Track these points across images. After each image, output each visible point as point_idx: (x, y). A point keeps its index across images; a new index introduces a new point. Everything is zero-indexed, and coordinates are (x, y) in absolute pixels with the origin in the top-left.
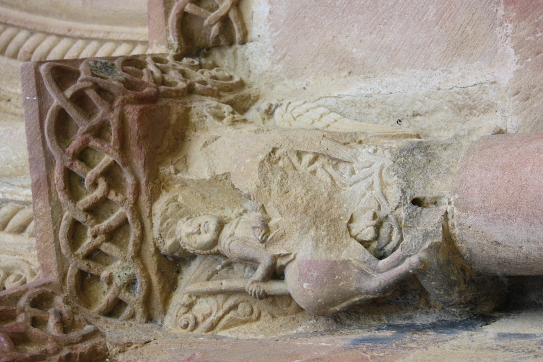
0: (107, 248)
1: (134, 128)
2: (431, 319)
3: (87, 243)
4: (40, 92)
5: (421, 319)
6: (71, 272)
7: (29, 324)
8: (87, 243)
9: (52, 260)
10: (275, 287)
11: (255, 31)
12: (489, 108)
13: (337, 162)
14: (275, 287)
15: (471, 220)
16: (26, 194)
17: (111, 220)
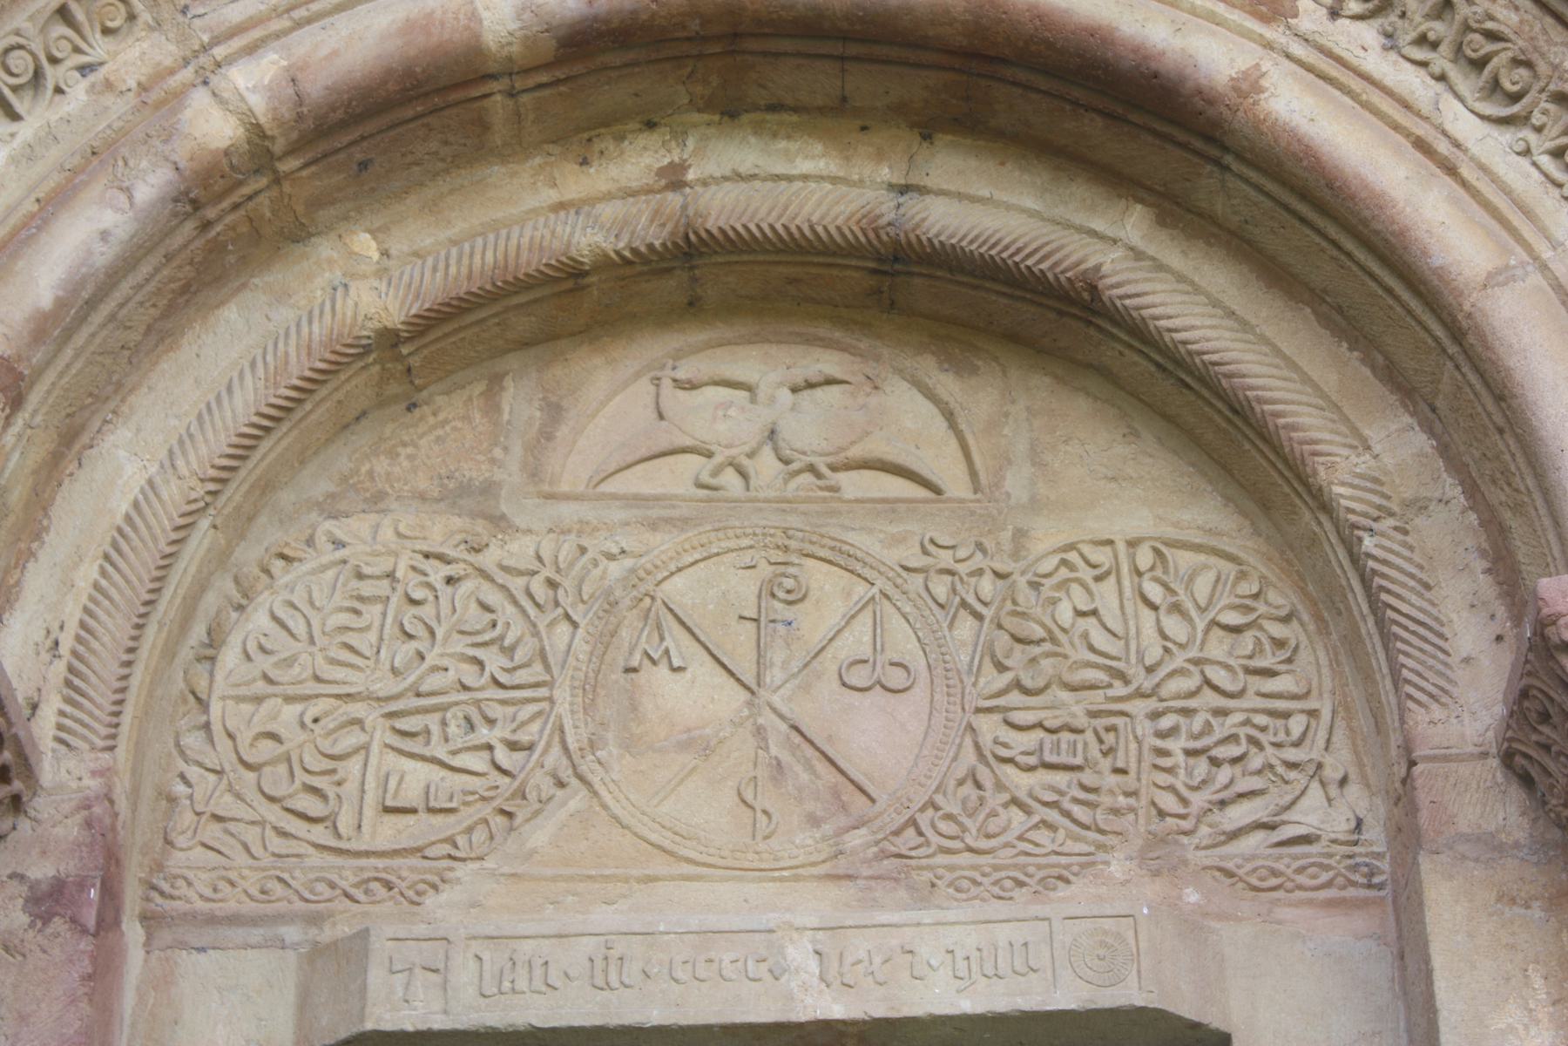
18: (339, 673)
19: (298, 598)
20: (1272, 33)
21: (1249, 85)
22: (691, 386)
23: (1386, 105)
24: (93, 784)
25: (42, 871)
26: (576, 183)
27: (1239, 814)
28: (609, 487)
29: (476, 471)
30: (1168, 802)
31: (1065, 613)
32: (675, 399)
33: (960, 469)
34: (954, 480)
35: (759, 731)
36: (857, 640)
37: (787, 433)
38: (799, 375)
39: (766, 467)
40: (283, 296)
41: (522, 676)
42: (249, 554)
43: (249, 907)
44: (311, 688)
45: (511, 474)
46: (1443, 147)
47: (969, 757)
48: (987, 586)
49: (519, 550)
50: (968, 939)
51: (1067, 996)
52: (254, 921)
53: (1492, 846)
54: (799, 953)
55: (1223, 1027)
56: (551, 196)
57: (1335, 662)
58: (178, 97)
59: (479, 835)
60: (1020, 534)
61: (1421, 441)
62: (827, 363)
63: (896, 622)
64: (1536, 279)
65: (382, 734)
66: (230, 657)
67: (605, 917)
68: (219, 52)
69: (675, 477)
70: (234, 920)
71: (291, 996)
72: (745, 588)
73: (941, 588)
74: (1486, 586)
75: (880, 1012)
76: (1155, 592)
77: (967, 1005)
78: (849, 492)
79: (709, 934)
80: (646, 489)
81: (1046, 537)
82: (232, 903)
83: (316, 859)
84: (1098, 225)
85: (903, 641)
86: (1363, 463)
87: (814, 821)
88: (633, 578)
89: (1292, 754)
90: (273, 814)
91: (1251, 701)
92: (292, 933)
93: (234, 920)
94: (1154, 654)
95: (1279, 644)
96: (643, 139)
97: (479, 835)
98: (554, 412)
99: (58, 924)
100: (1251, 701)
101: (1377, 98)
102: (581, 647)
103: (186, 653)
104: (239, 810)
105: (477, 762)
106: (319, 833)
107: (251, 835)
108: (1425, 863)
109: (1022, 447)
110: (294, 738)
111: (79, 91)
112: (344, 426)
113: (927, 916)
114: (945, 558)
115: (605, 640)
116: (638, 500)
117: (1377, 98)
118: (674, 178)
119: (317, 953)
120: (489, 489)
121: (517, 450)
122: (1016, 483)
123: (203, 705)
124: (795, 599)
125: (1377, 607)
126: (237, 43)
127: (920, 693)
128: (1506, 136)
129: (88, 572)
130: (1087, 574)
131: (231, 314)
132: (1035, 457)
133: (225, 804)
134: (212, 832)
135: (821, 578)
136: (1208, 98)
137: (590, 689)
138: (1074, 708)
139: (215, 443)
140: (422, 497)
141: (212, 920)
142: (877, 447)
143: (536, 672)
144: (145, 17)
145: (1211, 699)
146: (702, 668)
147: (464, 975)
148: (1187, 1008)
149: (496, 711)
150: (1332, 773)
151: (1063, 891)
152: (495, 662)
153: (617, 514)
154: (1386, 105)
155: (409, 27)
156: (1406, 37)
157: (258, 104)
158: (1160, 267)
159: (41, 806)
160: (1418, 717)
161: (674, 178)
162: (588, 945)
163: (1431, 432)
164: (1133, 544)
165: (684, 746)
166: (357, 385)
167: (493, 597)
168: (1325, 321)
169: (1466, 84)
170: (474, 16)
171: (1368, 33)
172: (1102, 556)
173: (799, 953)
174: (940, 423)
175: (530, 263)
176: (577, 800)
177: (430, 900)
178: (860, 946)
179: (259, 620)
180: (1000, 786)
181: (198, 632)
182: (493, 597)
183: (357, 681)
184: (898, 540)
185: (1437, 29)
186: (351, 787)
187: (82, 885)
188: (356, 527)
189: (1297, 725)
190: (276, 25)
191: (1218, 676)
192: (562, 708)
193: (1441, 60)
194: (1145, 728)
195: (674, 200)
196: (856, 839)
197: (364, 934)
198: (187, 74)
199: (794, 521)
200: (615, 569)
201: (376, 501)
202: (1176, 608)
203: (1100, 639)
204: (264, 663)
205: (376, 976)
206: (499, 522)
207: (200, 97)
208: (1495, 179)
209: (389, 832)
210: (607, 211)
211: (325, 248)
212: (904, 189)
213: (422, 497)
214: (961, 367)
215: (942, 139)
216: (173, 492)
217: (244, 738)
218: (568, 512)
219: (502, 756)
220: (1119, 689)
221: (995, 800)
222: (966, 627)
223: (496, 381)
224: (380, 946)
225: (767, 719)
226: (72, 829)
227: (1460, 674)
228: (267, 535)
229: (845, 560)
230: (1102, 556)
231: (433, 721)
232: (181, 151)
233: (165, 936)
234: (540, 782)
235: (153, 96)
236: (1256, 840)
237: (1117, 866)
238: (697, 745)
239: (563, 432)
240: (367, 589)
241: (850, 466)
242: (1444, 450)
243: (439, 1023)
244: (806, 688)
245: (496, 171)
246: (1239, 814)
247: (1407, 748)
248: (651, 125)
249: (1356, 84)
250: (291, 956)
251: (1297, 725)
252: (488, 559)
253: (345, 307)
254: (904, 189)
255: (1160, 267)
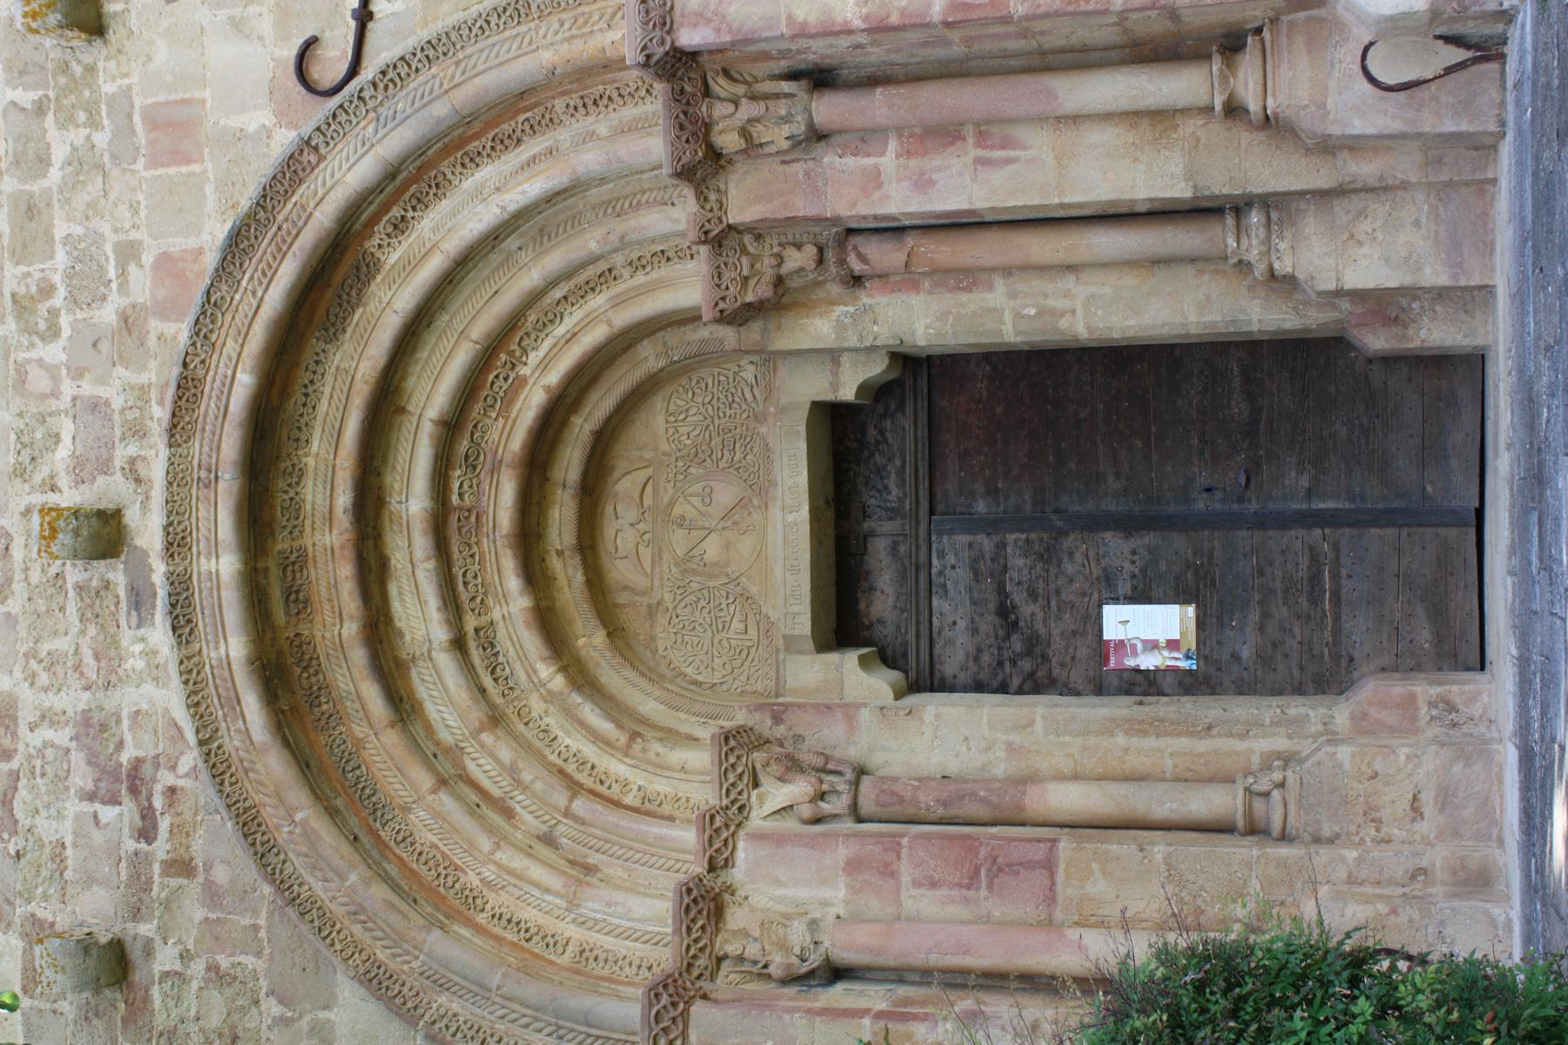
0: (699, 954)
1: (713, 911)
2: (816, 982)
3: (692, 952)
4: (681, 897)
5: (812, 983)
6: (685, 963)
7: (38, 507)
8: (692, 952)
9: (679, 959)
10: (765, 971)
11: (737, 864)
12: (833, 905)
13: (786, 926)
14: (765, 971)
15: (835, 950)
16: (669, 930)
17: (700, 944)
18: (705, 647)
19: (682, 659)
20: (531, 381)
21: (547, 389)
22: (617, 548)
23: (555, 351)
24: (744, 710)
25: (769, 722)
26: (562, 580)
27: (748, 395)
28: (649, 572)
29: (644, 610)
30: (745, 415)
31: (688, 442)
32: (621, 553)
33: (643, 471)
34: (650, 471)
35: (723, 529)
36: (696, 501)
37: (632, 521)
38: (613, 517)
39: (642, 526)
40: (598, 665)
41: (707, 596)
42: (668, 673)
43: (774, 668)
44: (710, 655)
45: (645, 600)
46: (569, 336)
47: (731, 470)
48: (680, 464)
49: (668, 597)
50: (786, 472)
51: (803, 446)
52: (778, 667)
53: (765, 331)
54: (791, 518)
55: (808, 406)
56: (566, 589)
57: (704, 367)
58: (549, 692)
59: (754, 606)
60: (664, 454)
61: (645, 342)
62: (609, 510)
63: (691, 490)
64: (610, 313)
65: (724, 634)
66: (700, 678)
67: (778, 570)
68: (536, 681)
69: (646, 553)
70: (777, 672)
71: (799, 657)
72: (680, 533)
73: (681, 477)
74: (689, 327)
75: (807, 496)
76: (682, 417)
77: (805, 473)
78: (651, 503)
79: (785, 542)
80: (649, 560)
81: (664, 446)
82: (773, 674)
83: (760, 651)
84: (577, 430)
85: (697, 488)
86: (652, 359)
87: (750, 513)
88: (677, 565)
89: (731, 380)
90: (747, 663)
91: (715, 391)
92: (781, 657)
93: (777, 672)
94: (701, 417)
95: (698, 382)
96: (548, 561)
97: (754, 606)
98: (626, 588)
99: (784, 717)
100: (715, 391)
101: (552, 354)
102: (698, 579)
103: (699, 690)
104: (746, 674)
105: (732, 608)
106: (753, 650)
107: (753, 669)
108: (770, 349)
109: (637, 453)
110: (725, 658)
111: (547, 720)
112: (631, 648)
113: (780, 483)
114: (671, 476)
115: (695, 573)
116: (653, 563)
117: (552, 354)
118: (560, 553)
119: (788, 649)
120: (649, 606)
121: (637, 598)
122: (648, 455)
123: (715, 684)
124: (683, 518)
125: (695, 356)
126: (533, 676)
127: (712, 484)
128: (566, 319)
129: (682, 715)
130: (677, 435)
131: (603, 679)
132: (640, 449)
133: (744, 678)
134: (752, 681)
135: (678, 510)
136: (550, 400)
137: (711, 577)
138: (716, 440)
139: (643, 682)
140: (652, 625)
141: (778, 679)
142: (636, 495)
143: (705, 592)
144: (525, 702)
145: (714, 402)
146: (704, 545)
147: (795, 609)
148: (806, 413)
149: (717, 602)
150: (737, 369)
151: (771, 445)
152: (702, 603)
153: (657, 569)
154: (555, 351)
155: (528, 627)
156: (535, 345)
157: (552, 669)
158: (590, 414)
159: (750, 723)
160: (728, 348)
161: (560, 553)
162: (788, 576)
163: (642, 340)
164: (667, 422)
165: (728, 550)
166: (418, 729)
167: (683, 604)
168: (608, 367)
169: (549, 329)
170: (524, 609)
171: (532, 355)
172: (671, 431)
173: (791, 518)
174: (629, 476)
175: (586, 594)
176: (743, 579)
177: (772, 619)
178: (788, 501)
179: (689, 670)
180: (740, 462)
181: (693, 687)
182: (683, 604)
183: (708, 642)
184: (666, 490)
185: (533, 336)
186: (739, 643)
187: (773, 711)
188: (661, 644)
189: (722, 378)
190: (527, 665)
191: (707, 400)
192: (716, 584)
193: (542, 335)
194: (723, 421)
195: (567, 553)
196: (755, 502)
197: (784, 636)
198: (542, 690)
199: (659, 519)
200: (674, 570)
201: (653, 639)
202: (687, 410)
203: (696, 433)
204: (702, 668)
205: (796, 632)
206: (659, 603)
207: (549, 686)
208: (579, 322)
209: (753, 633)
210: (570, 571)
211: (583, 653)
212: (564, 486)
213: (652, 625)
214: (612, 469)
215: (548, 475)
216: (658, 694)
217: (724, 673)
218: (656, 583)
219: (730, 601)
220: (711, 427)
221: (744, 463)
222: (692, 470)
223: (615, 605)
224: (788, 631)
225: (719, 527)
226: (757, 716)
227: (715, 335)
228: (663, 669)
229: (672, 504)
230: (671, 431)
231: (719, 621)
232: (566, 690)
233: (782, 691)
234: (738, 590)
235: (549, 698)
236: (755, 391)
237: (764, 430)
238: (727, 546)
239: (632, 585)
240: (679, 640)
241: (642, 503)
242: (648, 336)
243: (809, 615)
244: (710, 516)
245: (558, 604)
246: (748, 395)
247: (736, 351)
248: (544, 560)
249: (548, 359)
250: (788, 657)
251: (722, 378)
252: (671, 606)
253: (601, 647)
254: (564, 486)
255: (590, 414)
